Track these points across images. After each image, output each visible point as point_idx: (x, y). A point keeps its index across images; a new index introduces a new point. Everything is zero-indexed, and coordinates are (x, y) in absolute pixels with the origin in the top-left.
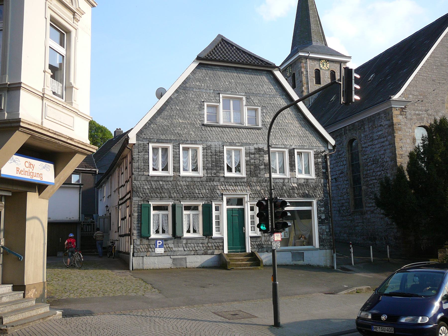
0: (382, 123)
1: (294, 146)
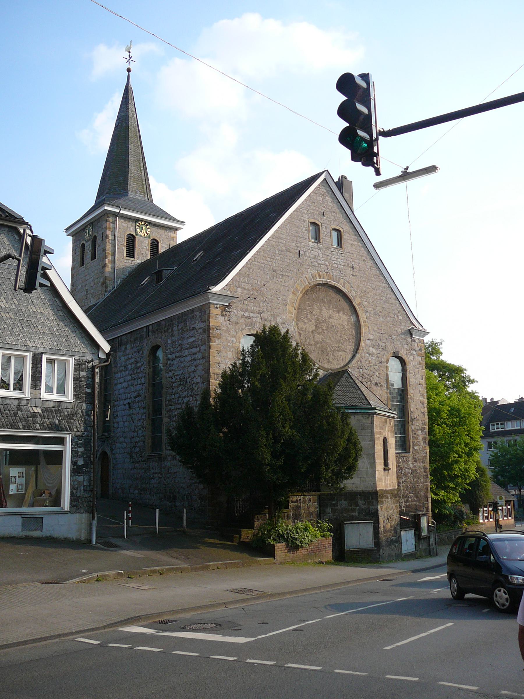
0: (195, 326)
1: (42, 349)
